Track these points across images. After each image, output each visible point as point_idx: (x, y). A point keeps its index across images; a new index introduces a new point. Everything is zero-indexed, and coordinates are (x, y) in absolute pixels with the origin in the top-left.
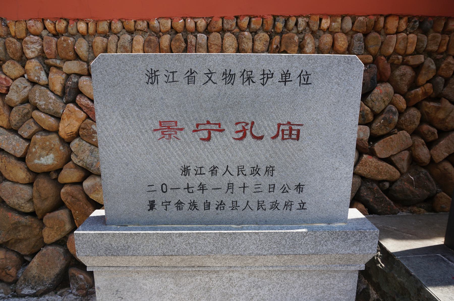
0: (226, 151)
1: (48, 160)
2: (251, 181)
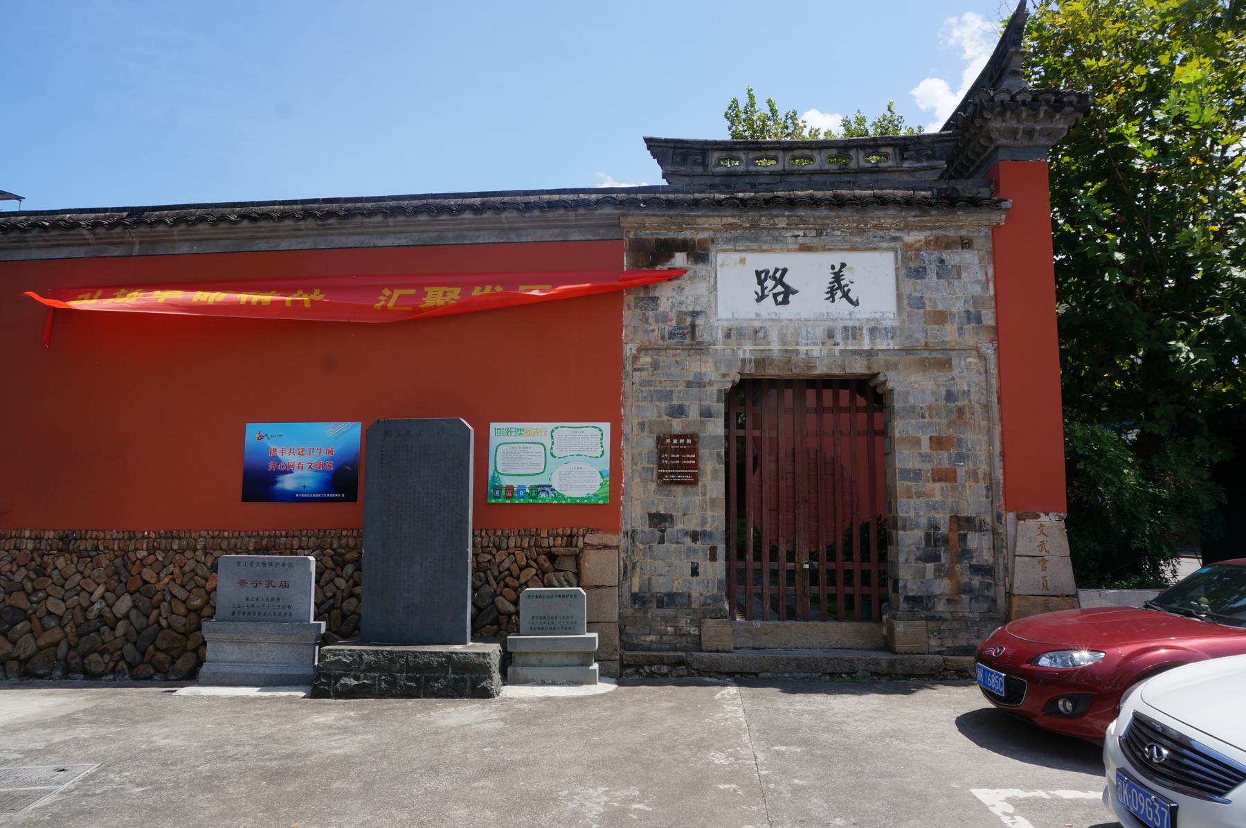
0: (263, 592)
1: (197, 602)
2: (271, 604)
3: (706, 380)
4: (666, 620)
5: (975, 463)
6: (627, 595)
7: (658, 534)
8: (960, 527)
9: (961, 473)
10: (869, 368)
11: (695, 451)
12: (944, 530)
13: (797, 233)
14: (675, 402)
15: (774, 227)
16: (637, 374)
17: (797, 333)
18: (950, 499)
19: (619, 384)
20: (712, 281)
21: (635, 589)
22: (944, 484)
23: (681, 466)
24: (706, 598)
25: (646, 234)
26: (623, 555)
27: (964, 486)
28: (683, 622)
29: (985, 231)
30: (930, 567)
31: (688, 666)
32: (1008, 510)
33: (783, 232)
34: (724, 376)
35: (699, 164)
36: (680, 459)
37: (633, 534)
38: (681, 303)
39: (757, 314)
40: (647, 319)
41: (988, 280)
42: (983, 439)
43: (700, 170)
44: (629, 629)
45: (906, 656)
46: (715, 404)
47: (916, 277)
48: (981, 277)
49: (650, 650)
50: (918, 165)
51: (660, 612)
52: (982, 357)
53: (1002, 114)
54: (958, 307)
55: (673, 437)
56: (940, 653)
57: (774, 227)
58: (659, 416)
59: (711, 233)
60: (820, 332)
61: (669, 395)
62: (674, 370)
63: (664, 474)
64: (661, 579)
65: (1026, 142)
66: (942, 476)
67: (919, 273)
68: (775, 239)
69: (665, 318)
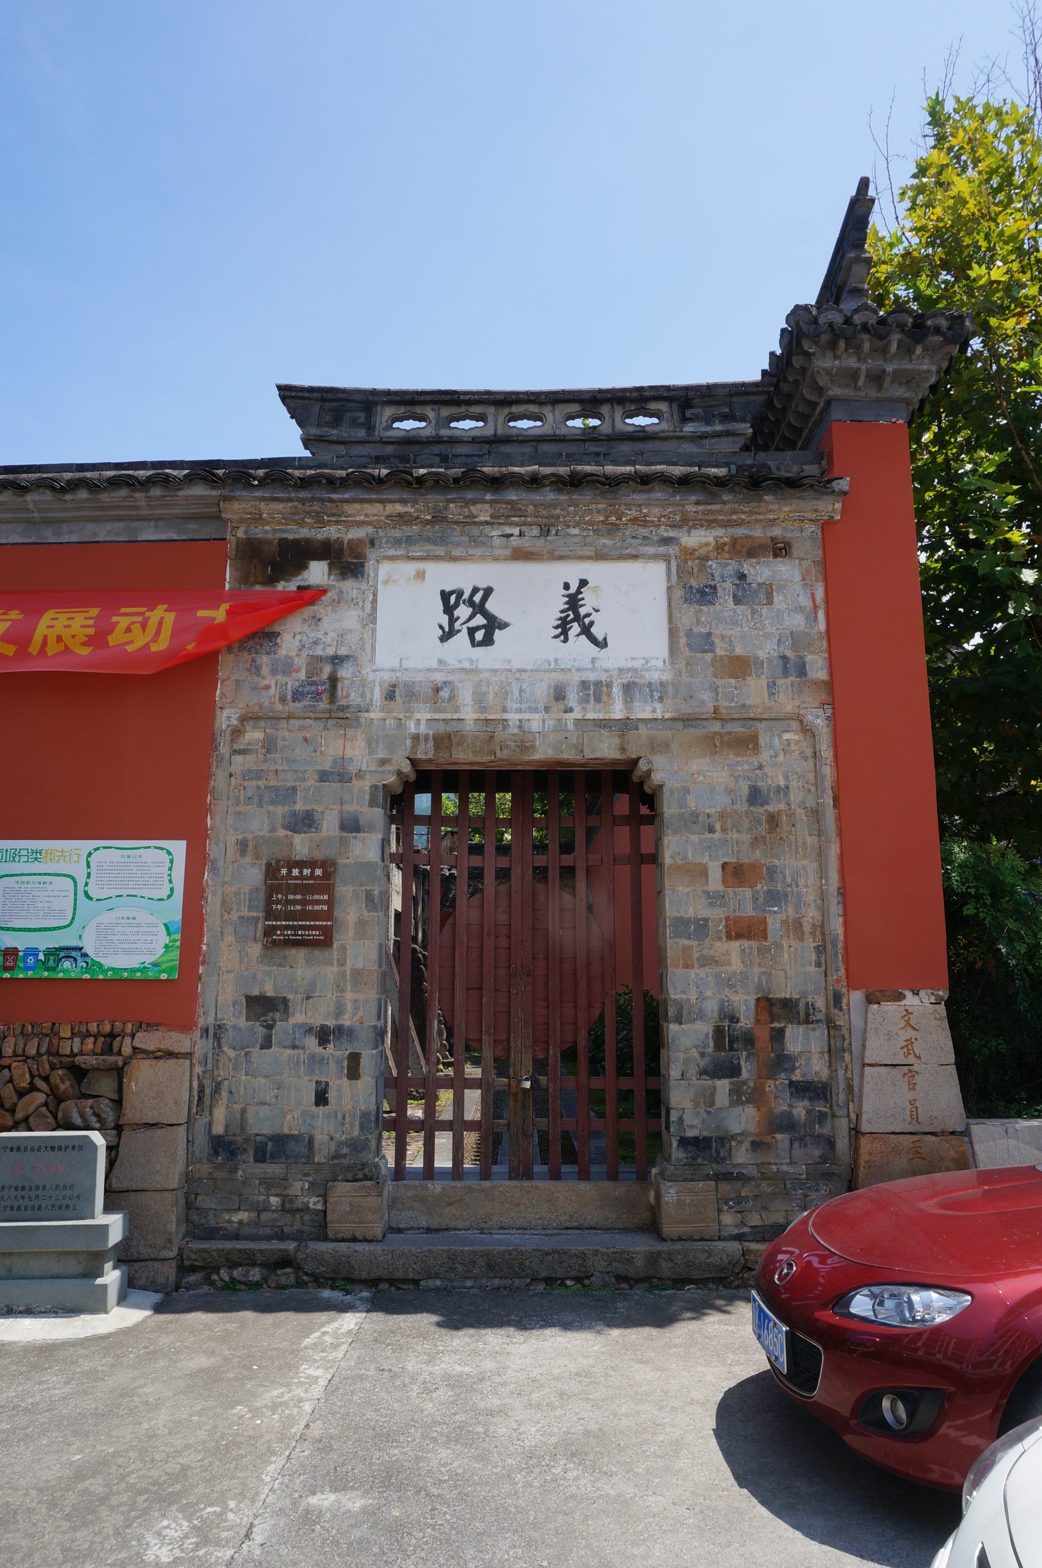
3: (353, 769)
4: (268, 1184)
5: (797, 908)
6: (202, 1142)
7: (261, 1031)
8: (773, 1018)
9: (774, 924)
10: (623, 750)
11: (329, 889)
12: (746, 1021)
13: (508, 530)
14: (300, 806)
15: (470, 521)
16: (238, 759)
17: (504, 692)
18: (756, 970)
19: (206, 775)
20: (368, 606)
21: (218, 1129)
22: (746, 943)
23: (304, 915)
24: (340, 1144)
25: (262, 532)
26: (198, 1069)
27: (779, 946)
28: (297, 1187)
29: (810, 529)
30: (723, 1085)
31: (298, 1268)
32: (851, 986)
33: (487, 529)
34: (383, 762)
35: (361, 425)
36: (304, 902)
37: (217, 1033)
38: (316, 643)
39: (440, 661)
40: (258, 669)
41: (815, 607)
42: (811, 866)
43: (361, 434)
44: (205, 1202)
45: (678, 1246)
46: (365, 809)
47: (700, 602)
48: (805, 601)
49: (236, 1237)
50: (708, 429)
51: (260, 1169)
52: (807, 731)
53: (833, 345)
54: (767, 650)
55: (291, 864)
56: (739, 1238)
57: (470, 521)
58: (273, 830)
59: (370, 530)
60: (542, 691)
61: (289, 794)
62: (301, 752)
63: (275, 928)
64: (264, 1112)
65: (872, 393)
66: (743, 930)
67: (706, 595)
68: (474, 541)
69: (287, 667)
